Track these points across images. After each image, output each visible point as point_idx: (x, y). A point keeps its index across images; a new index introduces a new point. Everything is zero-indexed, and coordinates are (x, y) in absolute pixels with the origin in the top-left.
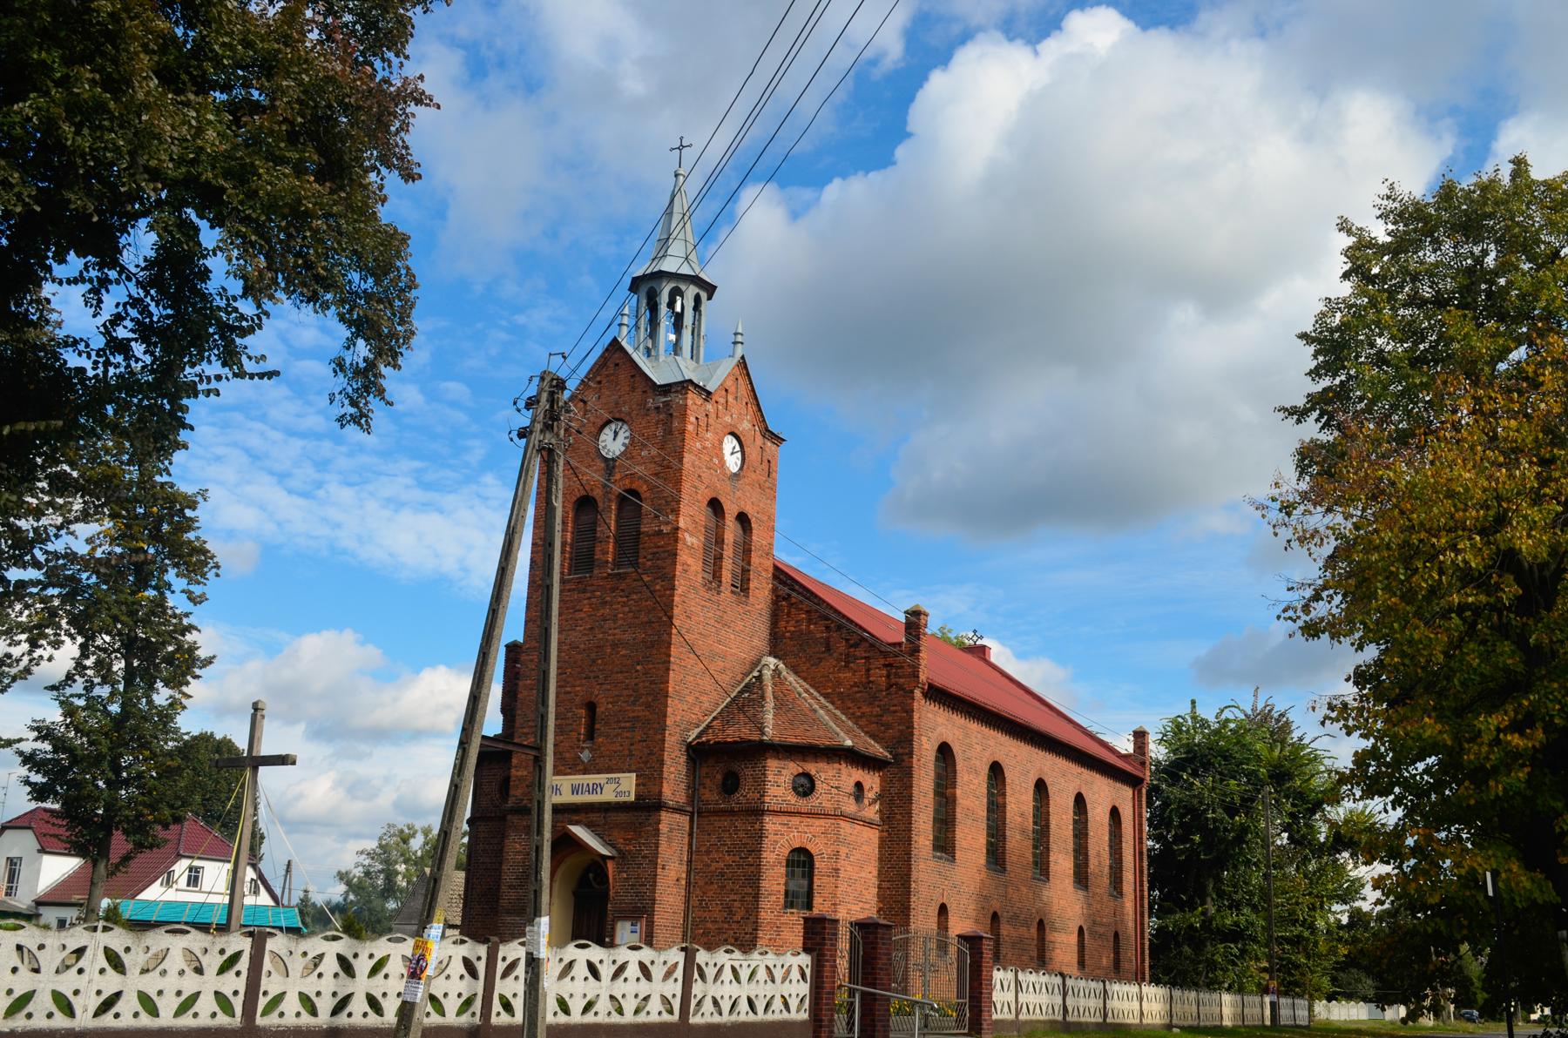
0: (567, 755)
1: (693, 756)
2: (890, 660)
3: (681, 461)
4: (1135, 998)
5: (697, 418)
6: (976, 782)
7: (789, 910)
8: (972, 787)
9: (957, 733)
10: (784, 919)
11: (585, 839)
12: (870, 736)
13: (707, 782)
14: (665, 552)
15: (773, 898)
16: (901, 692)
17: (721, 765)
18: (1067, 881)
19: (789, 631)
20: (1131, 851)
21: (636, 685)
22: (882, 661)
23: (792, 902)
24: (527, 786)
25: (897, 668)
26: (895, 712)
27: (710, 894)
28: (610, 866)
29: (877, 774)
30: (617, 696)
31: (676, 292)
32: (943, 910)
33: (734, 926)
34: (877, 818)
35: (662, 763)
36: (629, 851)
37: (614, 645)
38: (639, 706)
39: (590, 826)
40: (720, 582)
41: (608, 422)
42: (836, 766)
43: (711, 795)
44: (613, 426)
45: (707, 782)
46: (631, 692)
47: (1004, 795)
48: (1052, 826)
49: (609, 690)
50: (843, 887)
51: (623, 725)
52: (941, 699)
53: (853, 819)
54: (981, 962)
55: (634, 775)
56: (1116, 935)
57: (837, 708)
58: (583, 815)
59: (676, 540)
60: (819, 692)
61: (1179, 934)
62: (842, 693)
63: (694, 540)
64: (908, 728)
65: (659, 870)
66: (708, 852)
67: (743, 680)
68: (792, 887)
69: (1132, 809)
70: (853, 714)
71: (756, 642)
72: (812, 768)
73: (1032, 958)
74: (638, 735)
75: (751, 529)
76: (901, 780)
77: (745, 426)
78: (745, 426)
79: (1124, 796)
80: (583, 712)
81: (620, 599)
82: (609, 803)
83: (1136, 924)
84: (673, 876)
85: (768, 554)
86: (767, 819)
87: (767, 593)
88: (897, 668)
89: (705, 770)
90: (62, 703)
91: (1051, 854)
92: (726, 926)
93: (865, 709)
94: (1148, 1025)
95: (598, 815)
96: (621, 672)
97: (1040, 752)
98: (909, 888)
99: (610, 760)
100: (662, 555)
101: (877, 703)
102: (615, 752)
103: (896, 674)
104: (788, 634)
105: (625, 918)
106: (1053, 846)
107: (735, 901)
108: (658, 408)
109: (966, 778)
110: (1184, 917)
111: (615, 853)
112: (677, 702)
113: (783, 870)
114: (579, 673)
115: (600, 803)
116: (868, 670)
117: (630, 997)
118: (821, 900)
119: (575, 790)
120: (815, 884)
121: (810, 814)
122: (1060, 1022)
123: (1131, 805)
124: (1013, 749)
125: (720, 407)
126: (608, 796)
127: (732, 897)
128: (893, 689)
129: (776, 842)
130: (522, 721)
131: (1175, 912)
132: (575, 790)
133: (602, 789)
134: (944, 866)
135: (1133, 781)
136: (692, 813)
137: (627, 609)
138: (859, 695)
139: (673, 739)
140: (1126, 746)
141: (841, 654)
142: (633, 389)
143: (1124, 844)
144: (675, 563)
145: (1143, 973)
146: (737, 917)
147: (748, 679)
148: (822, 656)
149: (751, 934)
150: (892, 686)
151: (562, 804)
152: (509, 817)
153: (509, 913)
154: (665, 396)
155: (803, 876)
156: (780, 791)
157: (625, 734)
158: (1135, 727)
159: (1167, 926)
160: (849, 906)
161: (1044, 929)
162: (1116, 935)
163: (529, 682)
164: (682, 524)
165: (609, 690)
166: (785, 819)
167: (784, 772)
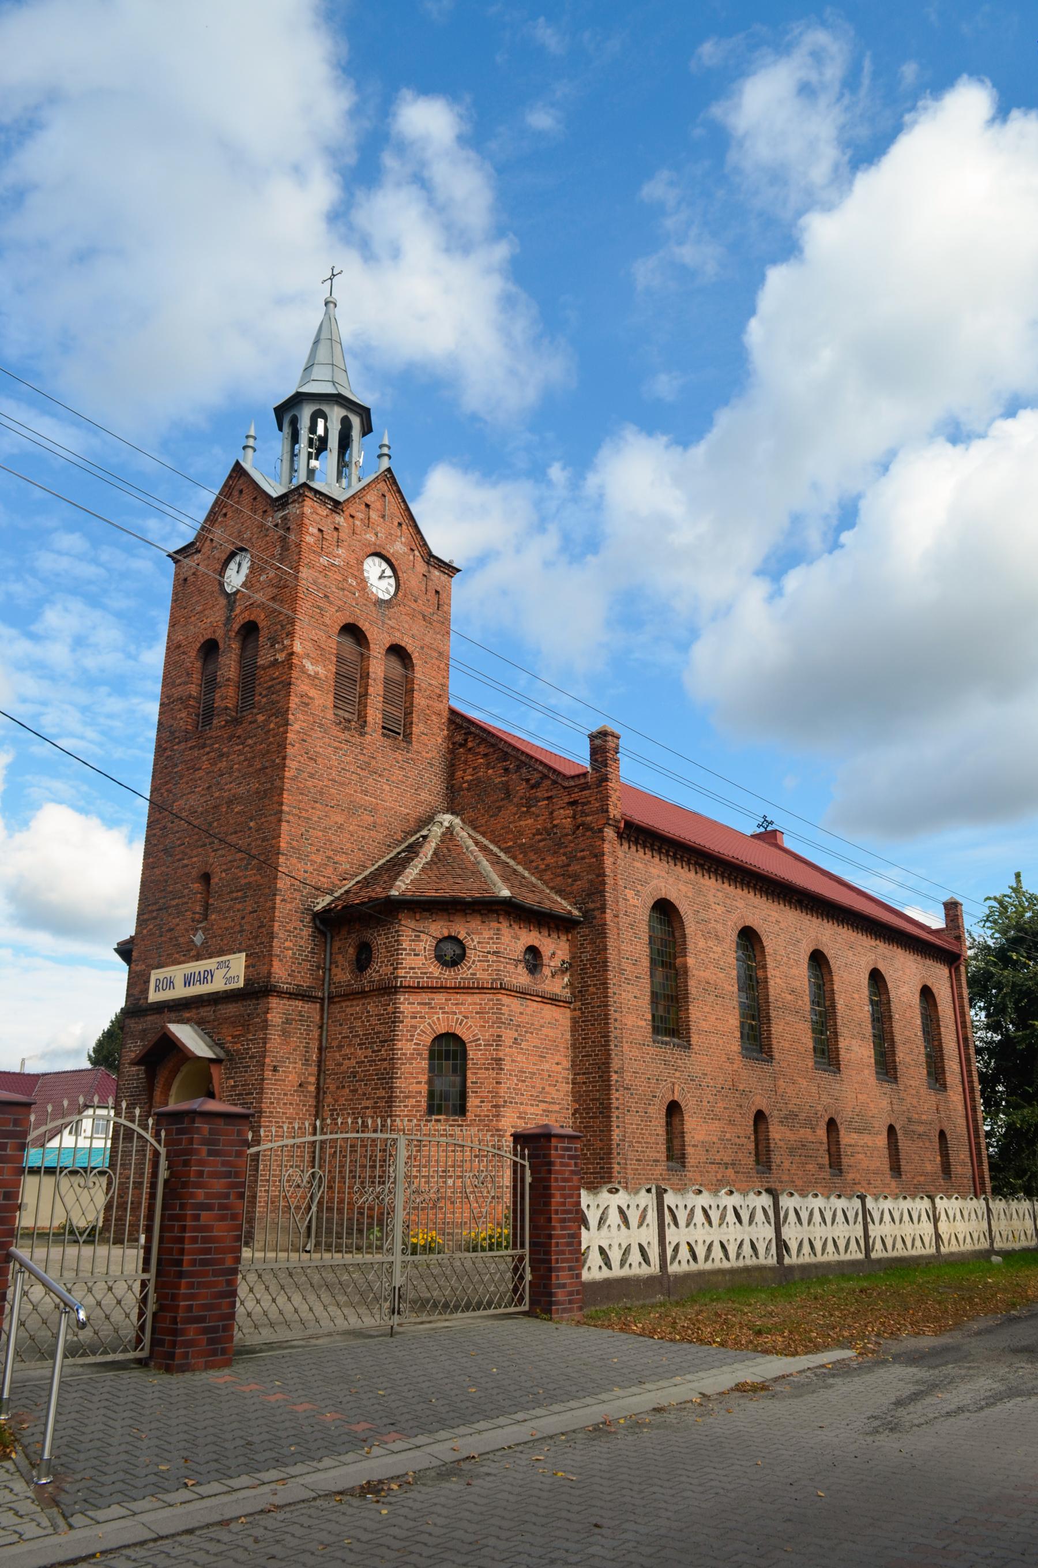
1: (321, 927)
2: (575, 796)
4: (924, 1217)
5: (320, 530)
6: (719, 950)
7: (434, 1117)
8: (711, 955)
9: (683, 888)
12: (556, 893)
13: (339, 958)
16: (589, 833)
17: (353, 936)
18: (866, 1072)
19: (467, 782)
20: (954, 1037)
21: (249, 845)
22: (566, 799)
23: (440, 1106)
25: (584, 804)
26: (583, 858)
27: (342, 1101)
28: (215, 1070)
29: (564, 938)
30: (230, 862)
32: (674, 1109)
34: (566, 993)
35: (271, 936)
37: (230, 803)
38: (252, 870)
39: (200, 1024)
40: (365, 722)
41: (232, 555)
42: (494, 925)
43: (343, 975)
44: (238, 559)
45: (339, 958)
47: (764, 967)
48: (839, 1007)
49: (223, 856)
50: (509, 1083)
51: (235, 895)
52: (660, 848)
53: (523, 994)
54: (549, 1180)
56: (942, 1134)
57: (519, 863)
58: (194, 1011)
59: (291, 667)
60: (499, 847)
61: (1028, 1130)
62: (524, 844)
63: (320, 670)
64: (598, 876)
65: (268, 1074)
66: (340, 1047)
67: (405, 839)
68: (440, 1085)
69: (950, 990)
70: (536, 868)
71: (866, 1008)
72: (460, 929)
73: (821, 1167)
75: (413, 666)
76: (592, 942)
77: (398, 548)
78: (398, 548)
79: (939, 977)
80: (197, 886)
83: (967, 1120)
84: (293, 1079)
85: (442, 694)
87: (440, 741)
89: (337, 944)
91: (841, 1039)
93: (550, 860)
94: (952, 1254)
95: (208, 1009)
96: (236, 833)
97: (814, 919)
98: (609, 1080)
103: (583, 812)
104: (465, 785)
106: (842, 1030)
107: (367, 1108)
109: (702, 944)
110: (1033, 1112)
111: (222, 1055)
112: (294, 861)
113: (425, 1064)
114: (197, 841)
117: (615, 1247)
118: (477, 1102)
120: (469, 1081)
121: (458, 989)
122: (771, 1269)
123: (948, 985)
124: (774, 914)
125: (358, 523)
126: (218, 985)
129: (415, 1027)
131: (1024, 1107)
133: (212, 976)
134: (671, 1053)
135: (950, 958)
136: (322, 999)
137: (242, 758)
139: (289, 906)
140: (936, 921)
143: (942, 1029)
144: (288, 694)
145: (983, 1184)
147: (414, 838)
148: (501, 804)
150: (578, 828)
151: (173, 1000)
154: (283, 510)
155: (454, 1071)
156: (418, 962)
158: (946, 898)
159: (1014, 1123)
160: (522, 1108)
161: (838, 1130)
162: (942, 1134)
164: (298, 647)
165: (223, 856)
166: (425, 997)
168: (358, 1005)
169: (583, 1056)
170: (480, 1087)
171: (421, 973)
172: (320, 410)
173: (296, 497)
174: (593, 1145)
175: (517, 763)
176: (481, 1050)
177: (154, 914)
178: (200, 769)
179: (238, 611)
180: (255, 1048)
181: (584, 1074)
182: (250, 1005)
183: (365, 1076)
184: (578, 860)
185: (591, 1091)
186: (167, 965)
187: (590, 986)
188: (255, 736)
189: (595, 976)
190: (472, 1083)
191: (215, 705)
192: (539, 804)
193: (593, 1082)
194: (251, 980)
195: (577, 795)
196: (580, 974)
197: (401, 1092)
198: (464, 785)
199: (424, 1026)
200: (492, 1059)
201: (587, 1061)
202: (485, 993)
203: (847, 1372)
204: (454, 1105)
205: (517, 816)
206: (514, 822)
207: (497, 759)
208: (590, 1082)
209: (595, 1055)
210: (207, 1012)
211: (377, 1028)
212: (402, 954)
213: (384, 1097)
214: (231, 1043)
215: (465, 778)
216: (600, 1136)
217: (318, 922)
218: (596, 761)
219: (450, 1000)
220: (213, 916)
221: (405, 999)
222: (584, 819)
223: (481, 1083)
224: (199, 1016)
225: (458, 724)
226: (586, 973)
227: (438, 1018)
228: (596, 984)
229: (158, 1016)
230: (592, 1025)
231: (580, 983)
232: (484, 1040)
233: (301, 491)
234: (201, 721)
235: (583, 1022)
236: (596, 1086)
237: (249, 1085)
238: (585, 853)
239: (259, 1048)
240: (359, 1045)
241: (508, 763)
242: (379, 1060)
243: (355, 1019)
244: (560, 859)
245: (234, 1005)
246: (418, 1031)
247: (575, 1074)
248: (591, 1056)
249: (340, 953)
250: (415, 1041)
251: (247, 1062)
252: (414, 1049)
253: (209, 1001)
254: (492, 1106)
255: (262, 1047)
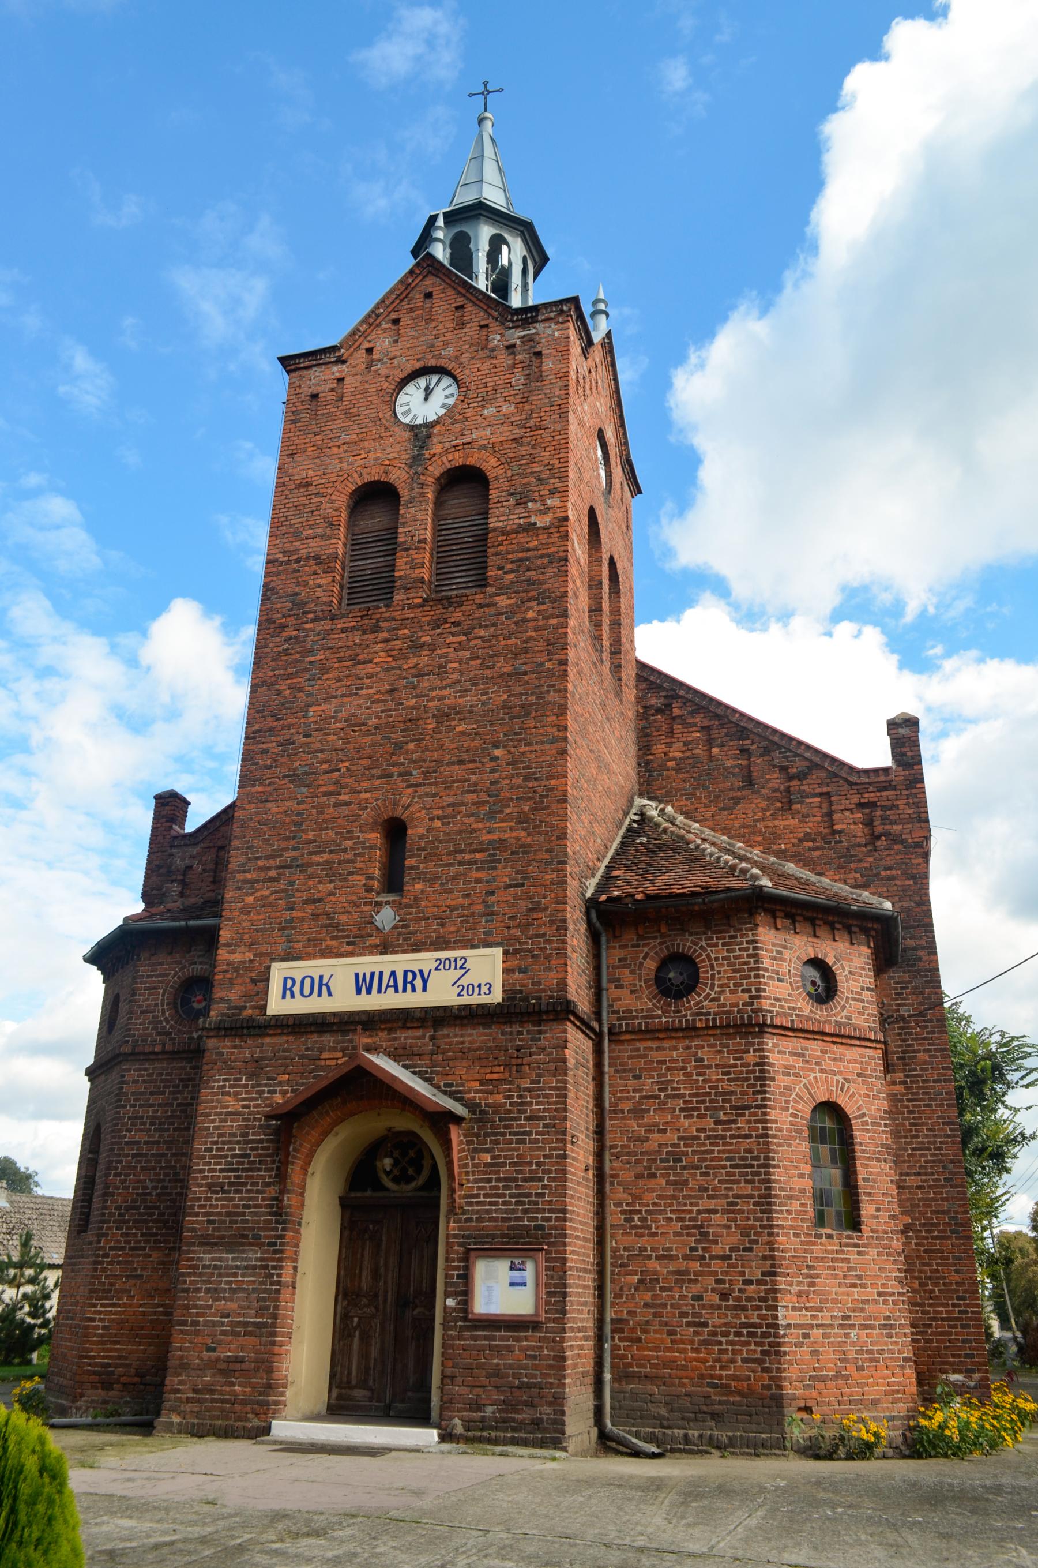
0: (344, 918)
2: (867, 797)
3: (564, 417)
10: (818, 1250)
11: (402, 1078)
14: (542, 556)
15: (795, 1206)
19: (674, 759)
22: (855, 799)
24: (254, 981)
31: (497, 243)
33: (716, 1266)
36: (496, 1107)
37: (441, 716)
38: (503, 821)
46: (483, 796)
55: (498, 952)
58: (384, 1035)
66: (638, 1112)
74: (504, 875)
76: (918, 992)
80: (375, 837)
81: (451, 639)
82: (445, 1008)
86: (770, 1042)
88: (884, 808)
90: (180, 1432)
92: (696, 1266)
95: (419, 1033)
99: (442, 925)
100: (539, 562)
101: (852, 865)
102: (453, 909)
104: (671, 764)
105: (494, 1252)
107: (715, 1212)
108: (513, 346)
115: (425, 1010)
116: (830, 814)
119: (363, 984)
127: (705, 1204)
128: (882, 843)
130: (242, 859)
132: (363, 984)
133: (425, 982)
138: (818, 853)
141: (775, 790)
142: (461, 325)
146: (722, 1247)
149: (759, 1282)
150: (878, 838)
151: (334, 1014)
152: (211, 1043)
153: (207, 1243)
157: (475, 875)
163: (259, 789)
167: (787, 954)
168: (675, 1048)
169: (913, 1149)
170: (873, 1188)
171: (789, 1008)
172: (500, 235)
173: (552, 315)
174: (944, 1278)
175: (764, 744)
176: (868, 1131)
177: (273, 873)
178: (370, 662)
179: (437, 449)
180: (538, 1103)
181: (916, 1174)
182: (520, 1033)
183: (701, 1160)
184: (882, 879)
185: (933, 1200)
186: (309, 956)
187: (918, 1051)
188: (493, 625)
189: (924, 1039)
190: (863, 1179)
191: (397, 574)
192: (808, 801)
193: (937, 1187)
194: (515, 992)
195: (872, 795)
196: (900, 1034)
197: (782, 1189)
198: (670, 764)
199: (800, 1089)
200: (882, 1145)
201: (922, 1155)
202: (866, 1047)
203: (54, 1477)
204: (838, 1213)
205: (768, 813)
206: (763, 820)
207: (726, 735)
208: (929, 1187)
209: (936, 1149)
210: (418, 1038)
211: (724, 1086)
212: (764, 977)
213: (751, 1196)
214: (477, 1091)
215: (671, 755)
216: (955, 1265)
217: (594, 915)
218: (814, 766)
219: (826, 1052)
220: (418, 887)
221: (775, 1045)
222: (888, 827)
223: (874, 1181)
224: (396, 1044)
225: (652, 683)
226: (910, 1034)
227: (816, 1078)
228: (929, 1050)
229: (291, 1038)
230: (925, 1106)
231: (900, 1046)
232: (870, 1116)
233: (565, 308)
234: (345, 597)
235: (909, 1100)
236: (941, 1193)
237: (530, 1164)
238: (894, 872)
239: (549, 1103)
240: (682, 1110)
241: (748, 742)
242: (732, 1137)
243: (668, 1069)
244: (851, 876)
245: (481, 1030)
246: (794, 1096)
247: (901, 1174)
248: (929, 1149)
249: (624, 967)
250: (791, 1111)
251: (521, 1126)
252: (792, 1123)
253: (483, 1016)
254: (890, 1217)
255: (556, 1103)
